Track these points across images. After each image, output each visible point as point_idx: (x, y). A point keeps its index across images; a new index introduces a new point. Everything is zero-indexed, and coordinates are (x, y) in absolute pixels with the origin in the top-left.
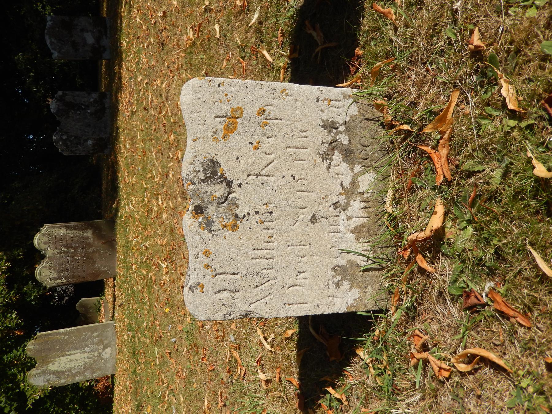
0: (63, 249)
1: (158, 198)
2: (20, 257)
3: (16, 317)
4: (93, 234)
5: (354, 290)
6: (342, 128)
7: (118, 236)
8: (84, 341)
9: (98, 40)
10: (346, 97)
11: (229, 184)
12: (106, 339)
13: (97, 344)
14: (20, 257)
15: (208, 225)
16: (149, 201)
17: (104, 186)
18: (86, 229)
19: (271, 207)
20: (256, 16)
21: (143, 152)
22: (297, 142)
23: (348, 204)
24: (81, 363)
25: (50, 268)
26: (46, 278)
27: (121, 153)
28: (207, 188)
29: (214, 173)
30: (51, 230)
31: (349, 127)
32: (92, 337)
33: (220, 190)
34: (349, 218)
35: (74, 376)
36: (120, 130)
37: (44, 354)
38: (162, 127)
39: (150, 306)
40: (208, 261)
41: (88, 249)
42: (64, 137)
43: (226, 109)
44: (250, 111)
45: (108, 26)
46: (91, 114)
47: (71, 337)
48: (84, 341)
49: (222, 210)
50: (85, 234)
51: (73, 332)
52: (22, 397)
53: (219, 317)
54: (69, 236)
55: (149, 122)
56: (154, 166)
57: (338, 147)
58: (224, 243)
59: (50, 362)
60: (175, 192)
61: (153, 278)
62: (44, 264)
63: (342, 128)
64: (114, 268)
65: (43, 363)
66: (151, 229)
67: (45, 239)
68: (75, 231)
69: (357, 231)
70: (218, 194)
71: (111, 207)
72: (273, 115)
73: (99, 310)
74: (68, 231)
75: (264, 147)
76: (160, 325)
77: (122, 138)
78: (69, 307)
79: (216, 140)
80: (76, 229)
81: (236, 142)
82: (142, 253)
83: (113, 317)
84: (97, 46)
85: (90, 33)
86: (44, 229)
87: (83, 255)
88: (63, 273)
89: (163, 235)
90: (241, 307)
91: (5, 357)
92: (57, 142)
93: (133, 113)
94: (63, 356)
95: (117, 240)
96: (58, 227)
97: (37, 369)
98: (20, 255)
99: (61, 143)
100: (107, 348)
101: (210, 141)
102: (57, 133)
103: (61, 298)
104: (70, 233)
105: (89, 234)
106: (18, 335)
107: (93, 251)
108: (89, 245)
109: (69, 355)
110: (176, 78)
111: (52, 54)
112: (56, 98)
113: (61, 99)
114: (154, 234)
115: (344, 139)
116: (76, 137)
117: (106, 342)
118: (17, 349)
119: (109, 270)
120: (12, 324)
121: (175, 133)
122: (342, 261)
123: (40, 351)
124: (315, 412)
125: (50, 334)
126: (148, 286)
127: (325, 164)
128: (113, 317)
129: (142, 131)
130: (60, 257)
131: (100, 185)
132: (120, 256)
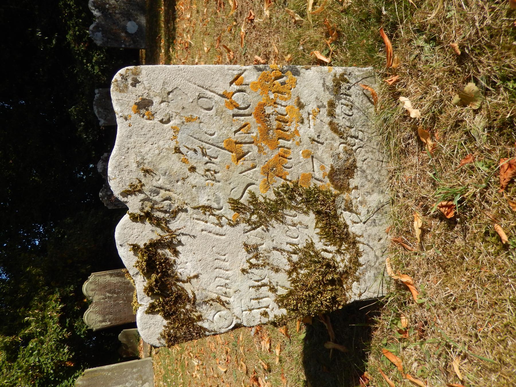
0: (108, 294)
2: (71, 295)
3: (68, 352)
8: (125, 377)
12: (145, 374)
13: (137, 379)
14: (71, 295)
25: (96, 313)
26: (93, 321)
30: (98, 278)
32: (132, 373)
41: (129, 293)
47: (114, 374)
48: (125, 376)
51: (115, 368)
54: (113, 283)
62: (90, 309)
67: (93, 287)
68: (118, 278)
74: (112, 278)
80: (118, 276)
86: (92, 278)
92: (103, 197)
96: (103, 275)
99: (106, 198)
100: (145, 383)
102: (103, 190)
106: (70, 367)
111: (99, 121)
112: (102, 160)
117: (145, 377)
118: (67, 380)
120: (64, 358)
124: (358, 383)
125: (96, 371)
130: (104, 302)
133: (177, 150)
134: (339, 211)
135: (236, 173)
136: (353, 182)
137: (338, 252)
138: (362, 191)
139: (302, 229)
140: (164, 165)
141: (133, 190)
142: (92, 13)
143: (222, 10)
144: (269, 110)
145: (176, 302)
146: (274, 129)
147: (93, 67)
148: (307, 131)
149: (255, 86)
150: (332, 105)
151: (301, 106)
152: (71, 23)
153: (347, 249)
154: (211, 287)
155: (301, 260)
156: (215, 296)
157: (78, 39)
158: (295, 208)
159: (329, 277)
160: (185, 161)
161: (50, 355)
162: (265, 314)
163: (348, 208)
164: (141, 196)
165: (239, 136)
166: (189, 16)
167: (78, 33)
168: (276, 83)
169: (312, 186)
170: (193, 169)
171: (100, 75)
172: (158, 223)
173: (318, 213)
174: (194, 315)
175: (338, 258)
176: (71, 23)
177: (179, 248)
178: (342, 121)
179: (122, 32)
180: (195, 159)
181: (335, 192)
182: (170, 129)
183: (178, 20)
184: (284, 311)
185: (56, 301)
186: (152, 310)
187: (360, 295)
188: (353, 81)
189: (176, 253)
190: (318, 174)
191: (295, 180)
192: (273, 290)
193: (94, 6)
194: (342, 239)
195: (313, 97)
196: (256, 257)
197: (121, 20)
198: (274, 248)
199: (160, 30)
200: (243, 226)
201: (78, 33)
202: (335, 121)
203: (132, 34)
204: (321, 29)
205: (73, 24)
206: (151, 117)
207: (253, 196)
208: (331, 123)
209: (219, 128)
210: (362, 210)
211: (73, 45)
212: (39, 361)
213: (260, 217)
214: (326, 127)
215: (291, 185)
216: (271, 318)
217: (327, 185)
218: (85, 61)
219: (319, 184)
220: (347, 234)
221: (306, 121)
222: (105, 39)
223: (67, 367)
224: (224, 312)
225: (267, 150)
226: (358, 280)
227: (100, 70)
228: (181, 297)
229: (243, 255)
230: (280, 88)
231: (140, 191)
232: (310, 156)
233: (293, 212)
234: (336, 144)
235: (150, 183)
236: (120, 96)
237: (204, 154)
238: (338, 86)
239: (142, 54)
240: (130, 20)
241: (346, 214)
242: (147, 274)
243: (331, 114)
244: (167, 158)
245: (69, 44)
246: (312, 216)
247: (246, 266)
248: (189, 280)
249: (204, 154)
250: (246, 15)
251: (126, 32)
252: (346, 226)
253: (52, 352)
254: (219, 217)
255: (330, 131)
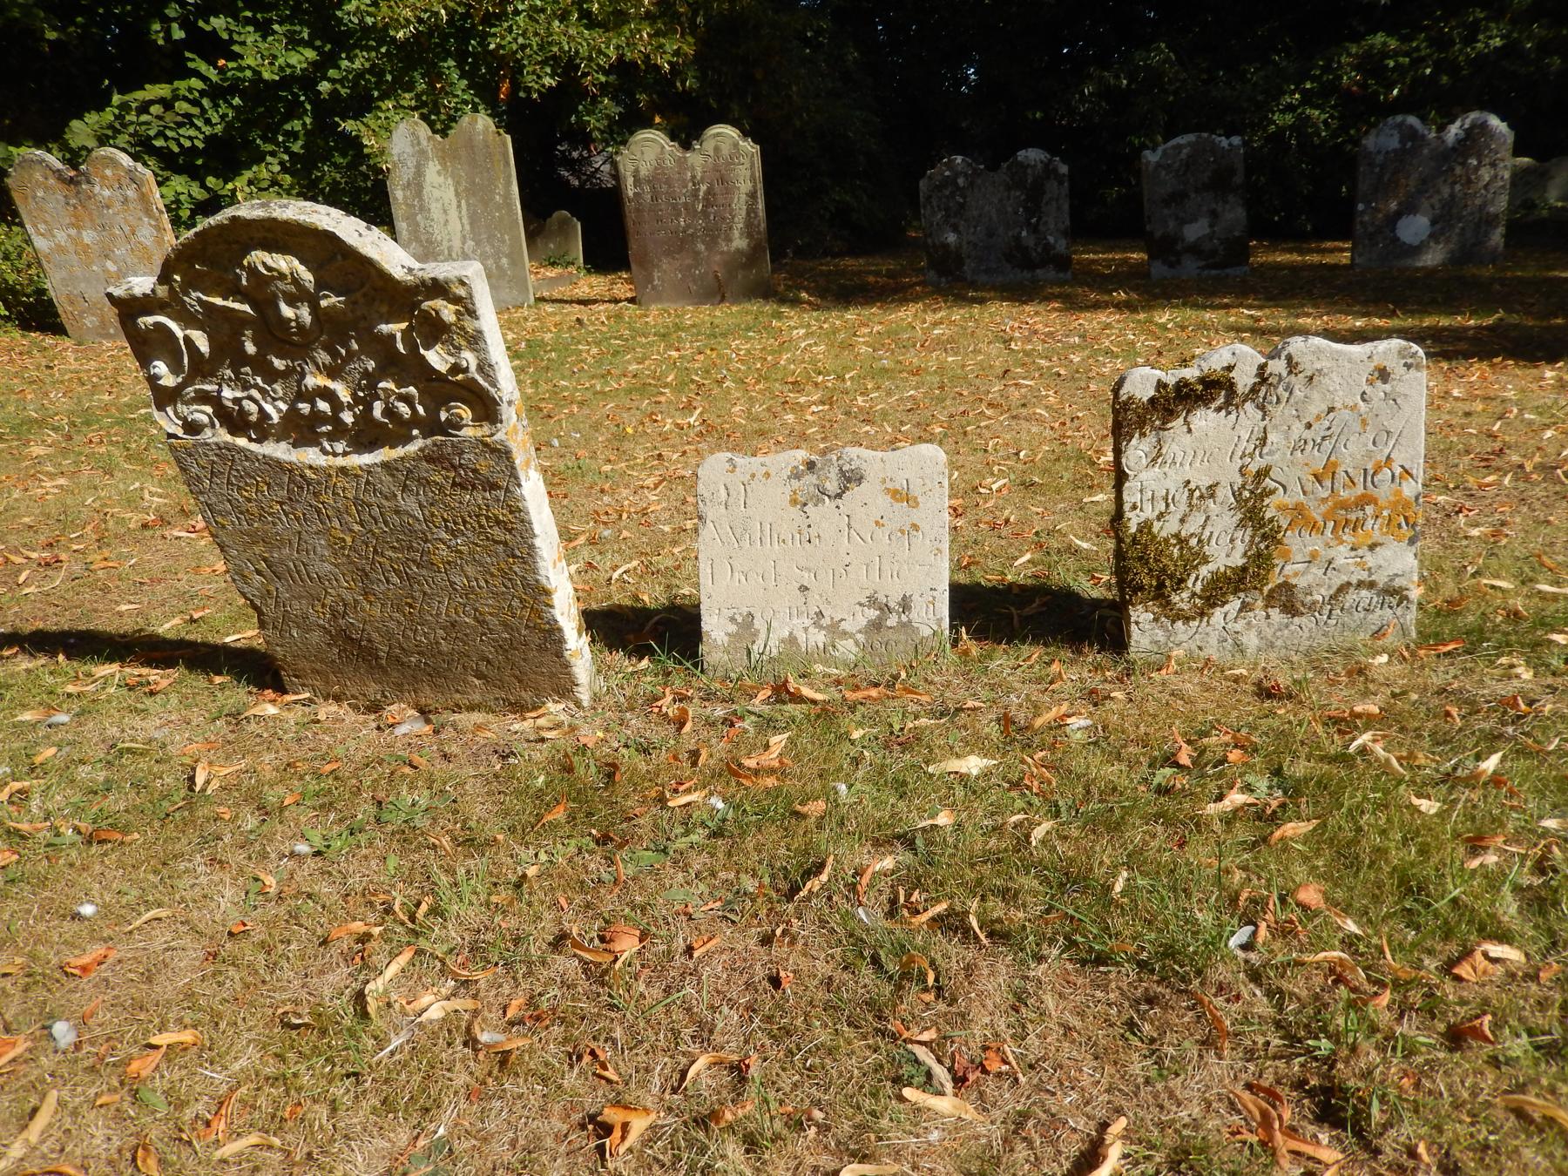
0: (703, 188)
1: (823, 403)
3: (543, 86)
4: (738, 250)
5: (726, 639)
6: (904, 618)
7: (734, 309)
9: (1195, 250)
10: (939, 621)
11: (839, 496)
15: (796, 476)
16: (816, 384)
17: (849, 263)
18: (749, 235)
19: (815, 541)
20: (1085, 545)
21: (919, 369)
22: (886, 567)
23: (821, 627)
24: (438, 233)
25: (660, 160)
27: (924, 311)
28: (833, 473)
29: (849, 480)
30: (746, 161)
31: (906, 626)
33: (832, 486)
34: (806, 629)
35: (411, 219)
36: (976, 309)
37: (463, 153)
38: (962, 409)
39: (602, 393)
40: (759, 476)
42: (961, 181)
43: (916, 490)
44: (916, 516)
45: (1228, 271)
46: (1018, 238)
47: (499, 208)
48: (490, 238)
49: (812, 489)
50: (736, 233)
52: (361, 104)
53: (701, 488)
55: (978, 381)
56: (889, 394)
57: (885, 615)
58: (777, 493)
59: (443, 164)
60: (836, 437)
61: (663, 399)
62: (670, 147)
63: (904, 618)
64: (658, 298)
65: (443, 150)
66: (761, 392)
67: (726, 150)
68: (744, 213)
69: (792, 640)
70: (828, 485)
71: (800, 288)
72: (913, 540)
73: (553, 264)
74: (743, 197)
75: (879, 531)
76: (572, 414)
77: (958, 314)
78: (575, 211)
79: (884, 481)
80: (748, 214)
81: (884, 501)
82: (707, 372)
83: (542, 299)
84: (1179, 247)
85: (1208, 231)
86: (750, 147)
87: (690, 231)
88: (647, 188)
89: (750, 417)
90: (710, 512)
91: (451, 63)
92: (950, 165)
93: (1007, 342)
94: (457, 194)
95: (725, 306)
97: (429, 139)
98: (683, 83)
101: (882, 475)
102: (969, 165)
103: (571, 164)
104: (740, 204)
105: (739, 242)
106: (499, 89)
107: (698, 253)
108: (712, 242)
109: (459, 206)
110: (1048, 432)
113: (1049, 171)
114: (751, 398)
115: (892, 621)
116: (962, 206)
118: (469, 87)
119: (654, 288)
120: (530, 78)
121: (945, 435)
122: (759, 624)
123: (470, 144)
125: (507, 163)
126: (642, 388)
127: (864, 600)
128: (542, 299)
129: (963, 366)
131: (853, 253)
132: (692, 314)
133: (1331, 409)
134: (1242, 595)
135: (1299, 474)
136: (1275, 613)
137: (1194, 594)
138: (1263, 624)
139: (1226, 550)
140: (1315, 395)
141: (1292, 365)
142: (1453, 122)
143: (1476, 463)
144: (1369, 510)
145: (1166, 410)
146: (1346, 517)
147: (1290, 108)
148: (1341, 555)
149: (1398, 493)
150: (1371, 585)
151: (1372, 547)
152: (1420, 43)
153: (1195, 605)
154: (1175, 447)
155: (1190, 548)
156: (1164, 451)
157: (1371, 64)
158: (1252, 542)
159: (1168, 583)
160: (1318, 418)
161: (535, 41)
162: (1134, 507)
163: (1245, 607)
164: (1284, 374)
165: (1341, 476)
166: (1456, 393)
167: (1392, 64)
168: (1403, 520)
169: (1276, 561)
170: (1309, 426)
171: (1265, 129)
172: (1254, 390)
173: (1244, 569)
174: (1147, 429)
175: (1185, 595)
176: (1420, 43)
177: (1223, 413)
178: (1351, 598)
179: (1400, 204)
180: (1319, 429)
181: (1266, 590)
182: (1361, 398)
183: (1445, 365)
184: (1133, 530)
185: (677, 53)
186: (1161, 385)
187: (1137, 623)
188: (1399, 611)
189: (1219, 410)
190: (1289, 569)
191: (1285, 541)
192: (1160, 516)
193: (1473, 126)
194: (1208, 599)
195: (1382, 562)
196: (1202, 497)
197: (1435, 200)
198: (1208, 518)
199: (1412, 313)
200: (1239, 481)
201: (1392, 64)
202: (1352, 590)
203: (1393, 230)
204: (1456, 594)
205: (1417, 49)
206: (1370, 383)
207: (1272, 492)
208: (1349, 584)
209: (1353, 453)
210: (1239, 626)
211: (1354, 51)
212: (517, 12)
213: (1247, 501)
214: (1345, 579)
215: (1279, 536)
216: (1128, 515)
217: (1275, 580)
218: (1308, 86)
219: (1277, 570)
220: (1214, 605)
221: (1353, 554)
222: (1379, 159)
223: (497, 83)
224: (1144, 462)
225: (1323, 508)
226: (1156, 620)
227: (1281, 130)
228: (1170, 415)
229: (1205, 482)
230: (1395, 523)
231: (1290, 372)
232: (1312, 559)
233: (1247, 539)
234: (1323, 591)
235: (1298, 382)
236: (1395, 351)
237: (1323, 438)
238: (1394, 593)
239: (1332, 251)
240: (1433, 223)
241: (1237, 604)
242: (1202, 380)
243: (1360, 584)
244: (1324, 399)
245: (1357, 38)
246: (1240, 562)
247: (1193, 486)
248: (1186, 422)
249: (1323, 438)
250: (1468, 504)
251: (1398, 215)
252: (1224, 603)
253: (541, 47)
254: (1251, 455)
255: (1339, 583)
